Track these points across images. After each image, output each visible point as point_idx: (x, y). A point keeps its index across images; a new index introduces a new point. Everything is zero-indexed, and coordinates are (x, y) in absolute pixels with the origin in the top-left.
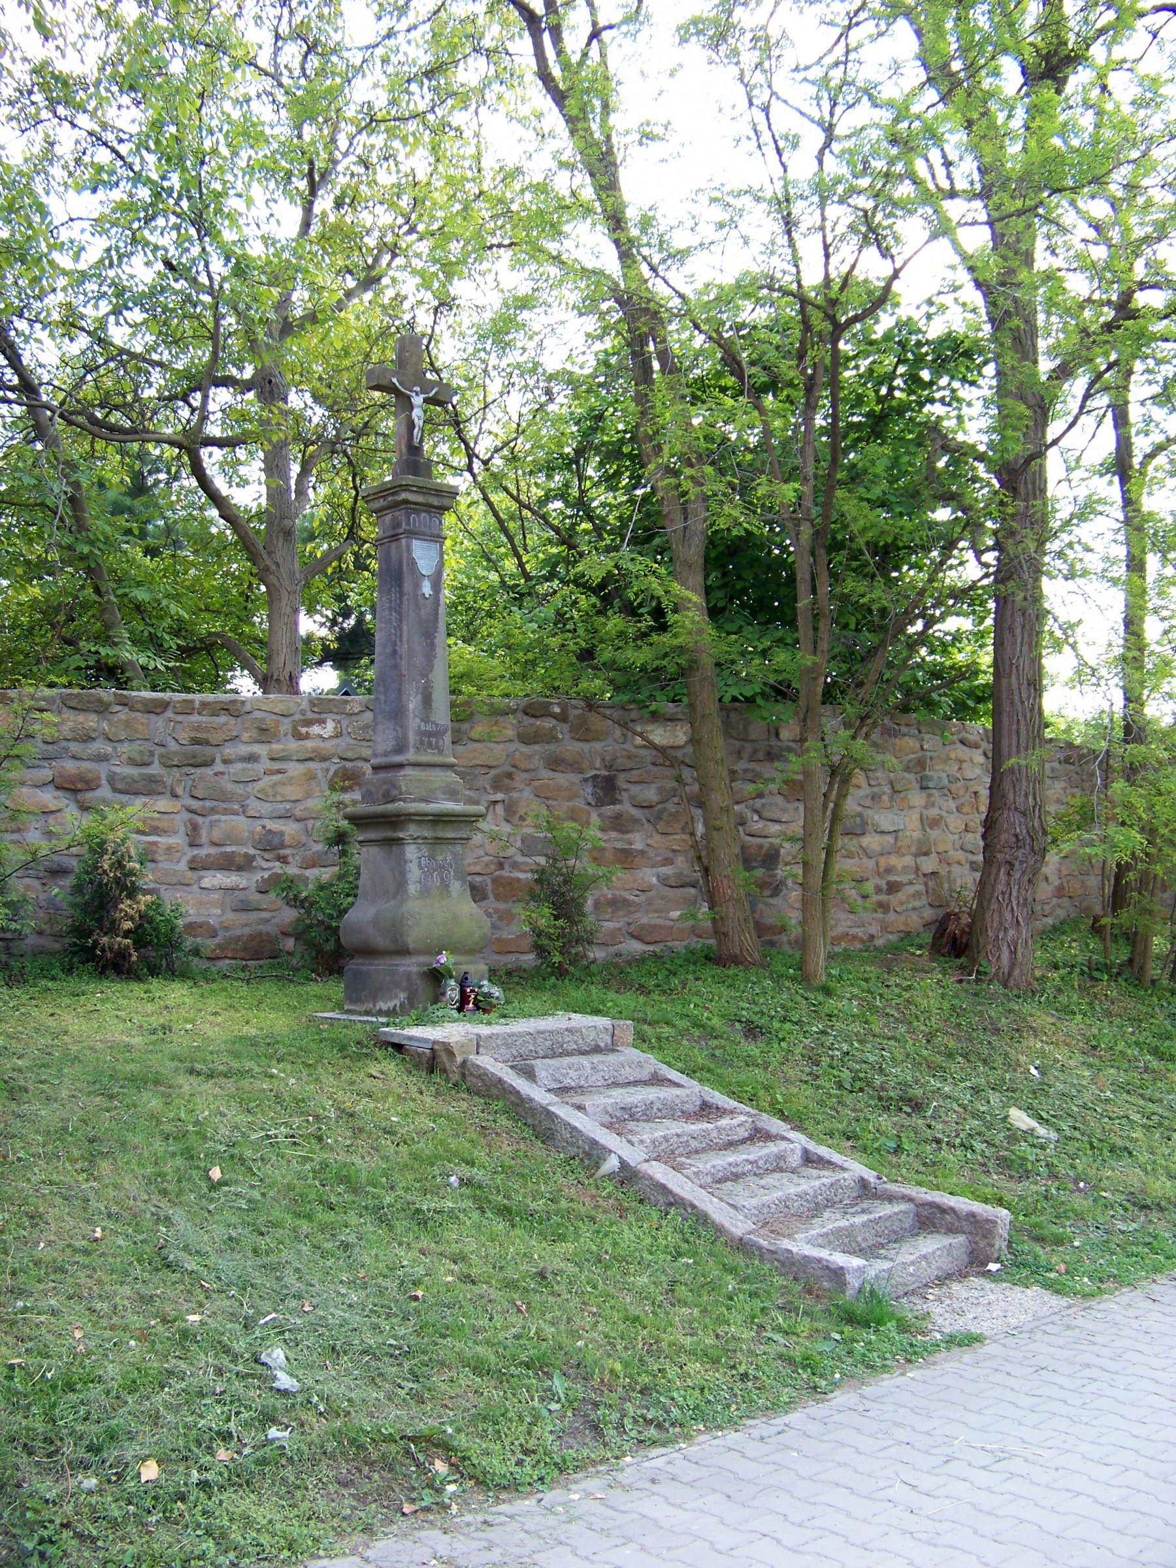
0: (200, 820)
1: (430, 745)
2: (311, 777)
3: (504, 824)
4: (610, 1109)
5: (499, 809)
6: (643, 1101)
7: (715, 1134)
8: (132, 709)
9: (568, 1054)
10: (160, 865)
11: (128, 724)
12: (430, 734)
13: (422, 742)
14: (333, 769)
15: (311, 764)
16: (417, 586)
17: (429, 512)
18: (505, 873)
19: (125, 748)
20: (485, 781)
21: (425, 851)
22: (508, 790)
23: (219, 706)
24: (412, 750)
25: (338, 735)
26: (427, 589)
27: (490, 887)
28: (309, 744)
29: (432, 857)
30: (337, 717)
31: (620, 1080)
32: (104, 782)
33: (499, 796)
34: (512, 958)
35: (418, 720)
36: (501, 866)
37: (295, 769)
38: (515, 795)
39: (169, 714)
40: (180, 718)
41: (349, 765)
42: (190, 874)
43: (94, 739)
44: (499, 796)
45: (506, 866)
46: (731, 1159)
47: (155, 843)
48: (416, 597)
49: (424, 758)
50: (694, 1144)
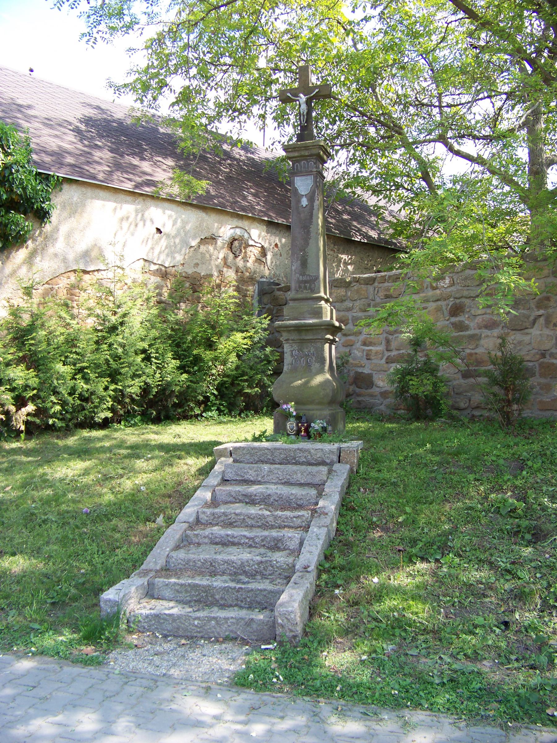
0: (390, 337)
1: (305, 288)
2: (439, 310)
3: (545, 329)
4: (233, 493)
5: (542, 320)
6: (262, 493)
7: (271, 519)
8: (360, 284)
9: (302, 464)
10: (373, 361)
11: (358, 291)
12: (306, 282)
13: (300, 287)
14: (451, 304)
15: (439, 303)
16: (299, 201)
17: (306, 160)
18: (545, 360)
19: (357, 303)
20: (532, 305)
21: (295, 347)
22: (546, 308)
23: (395, 277)
24: (293, 292)
25: (452, 284)
26: (304, 202)
27: (537, 369)
28: (438, 292)
29: (300, 350)
30: (451, 275)
31: (292, 481)
32: (350, 321)
33: (541, 312)
34: (548, 413)
35: (297, 275)
36: (543, 356)
37: (432, 306)
38: (550, 311)
39: (376, 284)
40: (381, 285)
41: (458, 301)
42: (386, 365)
43: (345, 300)
44: (541, 312)
45: (547, 356)
46: (229, 533)
47: (370, 350)
48: (297, 208)
49: (300, 296)
50: (250, 522)
